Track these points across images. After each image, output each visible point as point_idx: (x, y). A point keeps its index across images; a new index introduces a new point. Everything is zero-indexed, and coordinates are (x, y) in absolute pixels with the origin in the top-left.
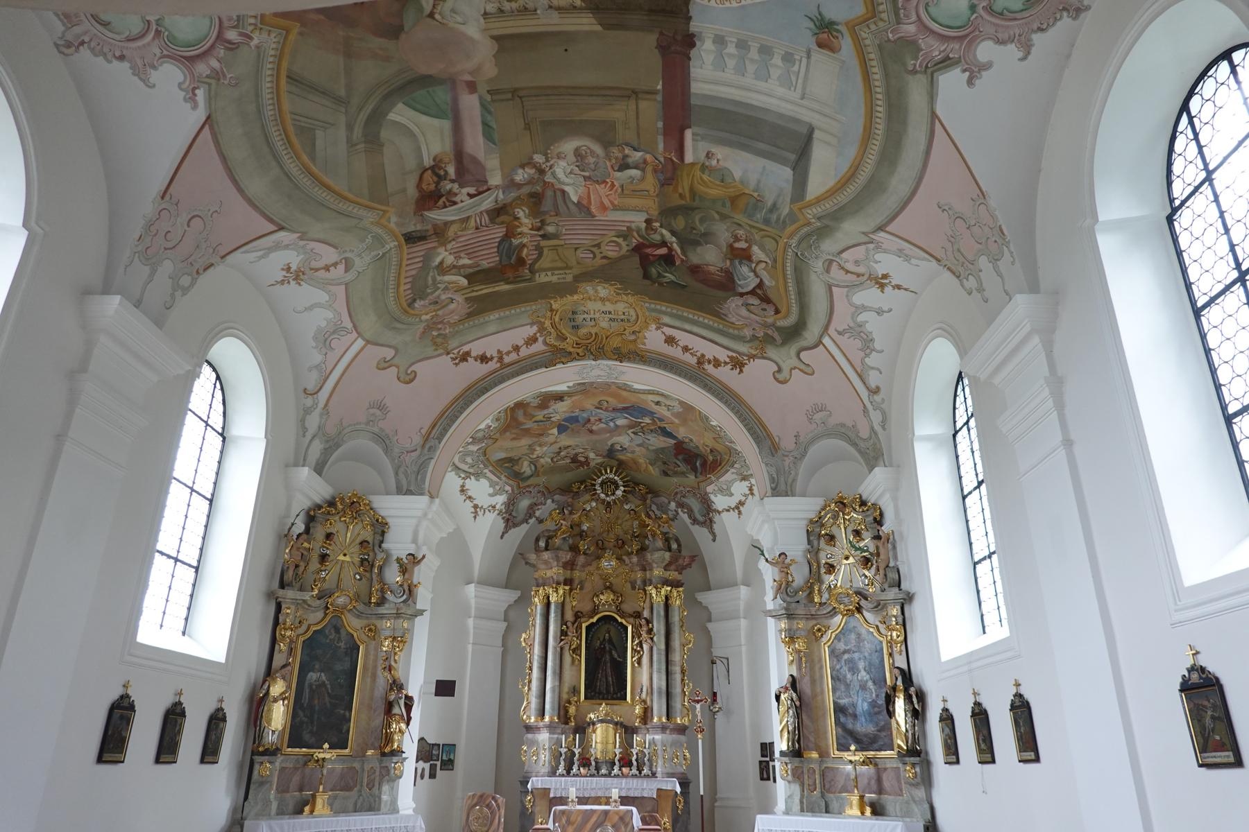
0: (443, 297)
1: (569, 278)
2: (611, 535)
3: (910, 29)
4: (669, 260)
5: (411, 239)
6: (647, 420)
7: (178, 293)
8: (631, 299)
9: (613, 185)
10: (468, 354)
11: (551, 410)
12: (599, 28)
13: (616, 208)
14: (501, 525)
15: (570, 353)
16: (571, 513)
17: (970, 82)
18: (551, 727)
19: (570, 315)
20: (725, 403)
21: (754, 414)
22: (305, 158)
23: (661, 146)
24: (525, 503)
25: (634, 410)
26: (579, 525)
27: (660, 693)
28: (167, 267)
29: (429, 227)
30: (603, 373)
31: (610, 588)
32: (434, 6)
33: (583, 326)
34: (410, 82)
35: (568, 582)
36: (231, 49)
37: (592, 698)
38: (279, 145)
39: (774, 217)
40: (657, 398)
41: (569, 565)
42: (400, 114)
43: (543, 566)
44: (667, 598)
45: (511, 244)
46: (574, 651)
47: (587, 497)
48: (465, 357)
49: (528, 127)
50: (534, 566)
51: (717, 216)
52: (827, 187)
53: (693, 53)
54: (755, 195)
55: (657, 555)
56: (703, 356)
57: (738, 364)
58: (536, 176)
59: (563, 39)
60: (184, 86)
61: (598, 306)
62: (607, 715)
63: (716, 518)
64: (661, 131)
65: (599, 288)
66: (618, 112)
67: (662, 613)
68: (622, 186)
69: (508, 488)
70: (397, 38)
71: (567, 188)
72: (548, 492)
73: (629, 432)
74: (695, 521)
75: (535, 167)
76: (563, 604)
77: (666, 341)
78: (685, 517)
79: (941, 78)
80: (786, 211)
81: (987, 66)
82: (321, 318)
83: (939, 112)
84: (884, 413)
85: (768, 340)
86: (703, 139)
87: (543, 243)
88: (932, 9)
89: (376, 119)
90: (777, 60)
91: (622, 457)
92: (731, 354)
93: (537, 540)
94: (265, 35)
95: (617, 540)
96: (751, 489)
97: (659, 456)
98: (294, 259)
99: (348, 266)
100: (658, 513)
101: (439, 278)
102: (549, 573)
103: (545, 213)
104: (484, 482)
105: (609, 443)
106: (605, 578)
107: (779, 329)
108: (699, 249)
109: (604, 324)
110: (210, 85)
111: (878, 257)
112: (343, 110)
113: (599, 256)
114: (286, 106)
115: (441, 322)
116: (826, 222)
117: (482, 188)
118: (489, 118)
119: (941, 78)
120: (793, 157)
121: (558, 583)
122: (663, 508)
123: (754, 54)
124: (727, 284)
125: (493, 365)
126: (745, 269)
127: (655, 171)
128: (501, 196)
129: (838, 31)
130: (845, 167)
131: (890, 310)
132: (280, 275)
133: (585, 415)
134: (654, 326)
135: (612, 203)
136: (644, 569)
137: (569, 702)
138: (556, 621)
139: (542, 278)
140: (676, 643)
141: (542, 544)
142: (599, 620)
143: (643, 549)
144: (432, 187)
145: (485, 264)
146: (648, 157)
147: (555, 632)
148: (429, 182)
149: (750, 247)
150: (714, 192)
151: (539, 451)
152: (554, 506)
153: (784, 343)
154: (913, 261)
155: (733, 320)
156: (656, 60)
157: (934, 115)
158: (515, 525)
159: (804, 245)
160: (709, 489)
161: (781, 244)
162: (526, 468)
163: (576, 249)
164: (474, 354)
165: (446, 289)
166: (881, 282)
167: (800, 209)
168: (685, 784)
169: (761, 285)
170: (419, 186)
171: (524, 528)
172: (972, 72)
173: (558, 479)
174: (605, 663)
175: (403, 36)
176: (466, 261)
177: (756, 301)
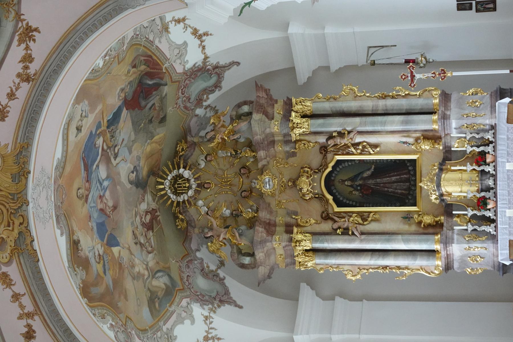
2: (236, 181)
6: (100, 142)
11: (90, 255)
14: (227, 308)
15: (20, 233)
16: (211, 229)
18: (447, 242)
20: (75, 48)
21: (88, 14)
24: (202, 283)
25: (88, 158)
26: (225, 219)
27: (406, 123)
30: (44, 194)
31: (294, 182)
35: (289, 229)
37: (415, 198)
40: (73, 131)
41: (270, 228)
43: (272, 258)
44: (304, 116)
46: (364, 220)
47: (192, 210)
50: (272, 269)
55: (256, 128)
56: (19, 75)
57: (28, 34)
62: (431, 181)
63: (213, 61)
67: (320, 121)
69: (184, 302)
72: (188, 257)
73: (114, 162)
74: (217, 86)
76: (313, 234)
78: (212, 97)
91: (144, 172)
93: (243, 266)
95: (241, 175)
96: (178, 21)
97: (143, 128)
100: (209, 128)
102: (280, 251)
104: (178, 331)
105: (129, 186)
106: (283, 187)
121: (291, 240)
122: (203, 122)
125: (37, 324)
133: (95, 215)
136: (273, 143)
137: (420, 223)
138: (332, 241)
140: (353, 105)
141: (247, 260)
142: (330, 193)
143: (250, 145)
147: (345, 241)
151: (139, 268)
152: (204, 249)
158: (227, 292)
160: (179, 69)
162: (160, 282)
168: (502, 94)
171: (230, 282)
173: (173, 245)
174: (377, 184)
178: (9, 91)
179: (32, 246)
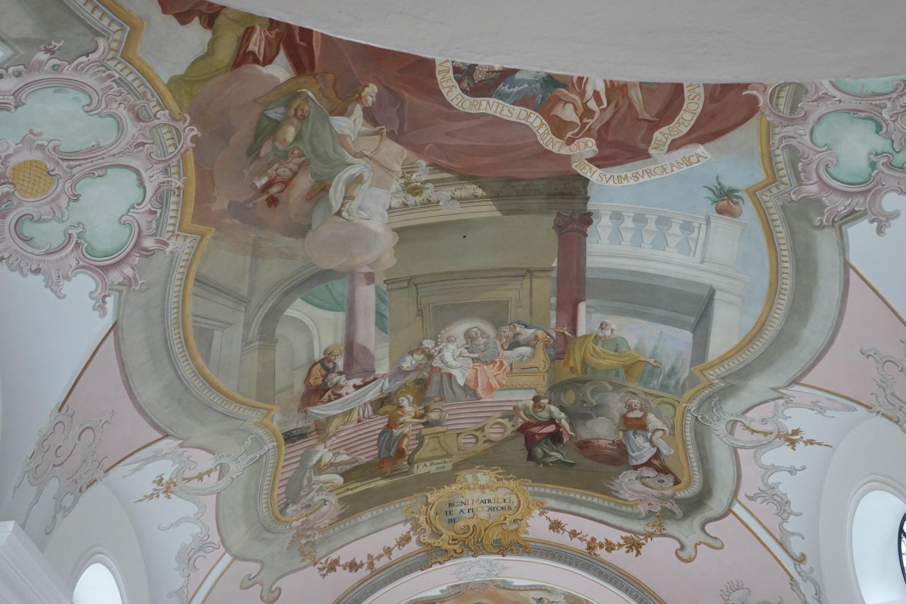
0: (316, 499)
1: (449, 467)
3: (812, 189)
4: (556, 438)
5: (291, 437)
7: (59, 516)
8: (513, 484)
9: (502, 364)
10: (336, 562)
12: (498, 214)
13: (503, 388)
15: (446, 551)
17: (880, 231)
19: (446, 508)
20: (626, 591)
22: (200, 360)
23: (553, 322)
28: (53, 486)
29: (311, 423)
32: (342, 205)
33: (460, 519)
34: (312, 277)
36: (147, 256)
38: (176, 347)
39: (673, 382)
42: (298, 309)
45: (392, 434)
48: (332, 567)
49: (420, 313)
51: (610, 387)
52: (730, 347)
53: (590, 230)
54: (652, 361)
56: (593, 539)
57: (634, 545)
58: (424, 362)
59: (463, 226)
60: (95, 295)
61: (477, 495)
65: (479, 475)
66: (512, 292)
70: (304, 237)
71: (453, 372)
75: (423, 352)
77: (551, 527)
79: (849, 230)
80: (686, 374)
81: (895, 215)
82: (186, 534)
83: (852, 261)
84: (815, 583)
85: (667, 514)
86: (597, 311)
87: (426, 431)
88: (831, 170)
89: (274, 315)
90: (675, 229)
92: (624, 534)
94: (181, 239)
98: (166, 468)
99: (223, 470)
101: (314, 478)
103: (430, 399)
107: (679, 501)
108: (589, 423)
109: (483, 514)
110: (121, 292)
111: (787, 412)
112: (243, 309)
113: (482, 440)
114: (190, 308)
115: (312, 528)
116: (731, 381)
117: (369, 377)
118: (383, 307)
119: (849, 230)
120: (692, 320)
123: (651, 225)
124: (619, 458)
125: (363, 572)
126: (639, 440)
127: (546, 346)
128: (387, 385)
130: (750, 324)
132: (150, 488)
134: (537, 512)
135: (500, 383)
139: (421, 469)
144: (320, 381)
145: (363, 459)
146: (540, 333)
148: (317, 378)
149: (645, 416)
150: (607, 363)
153: (686, 516)
154: (828, 413)
155: (626, 496)
156: (552, 240)
157: (847, 266)
159: (705, 407)
161: (680, 410)
163: (458, 435)
164: (342, 562)
165: (321, 489)
166: (791, 439)
167: (701, 371)
169: (657, 455)
170: (306, 381)
172: (880, 222)
175: (310, 235)
176: (345, 457)
177: (651, 473)
179: (435, 563)
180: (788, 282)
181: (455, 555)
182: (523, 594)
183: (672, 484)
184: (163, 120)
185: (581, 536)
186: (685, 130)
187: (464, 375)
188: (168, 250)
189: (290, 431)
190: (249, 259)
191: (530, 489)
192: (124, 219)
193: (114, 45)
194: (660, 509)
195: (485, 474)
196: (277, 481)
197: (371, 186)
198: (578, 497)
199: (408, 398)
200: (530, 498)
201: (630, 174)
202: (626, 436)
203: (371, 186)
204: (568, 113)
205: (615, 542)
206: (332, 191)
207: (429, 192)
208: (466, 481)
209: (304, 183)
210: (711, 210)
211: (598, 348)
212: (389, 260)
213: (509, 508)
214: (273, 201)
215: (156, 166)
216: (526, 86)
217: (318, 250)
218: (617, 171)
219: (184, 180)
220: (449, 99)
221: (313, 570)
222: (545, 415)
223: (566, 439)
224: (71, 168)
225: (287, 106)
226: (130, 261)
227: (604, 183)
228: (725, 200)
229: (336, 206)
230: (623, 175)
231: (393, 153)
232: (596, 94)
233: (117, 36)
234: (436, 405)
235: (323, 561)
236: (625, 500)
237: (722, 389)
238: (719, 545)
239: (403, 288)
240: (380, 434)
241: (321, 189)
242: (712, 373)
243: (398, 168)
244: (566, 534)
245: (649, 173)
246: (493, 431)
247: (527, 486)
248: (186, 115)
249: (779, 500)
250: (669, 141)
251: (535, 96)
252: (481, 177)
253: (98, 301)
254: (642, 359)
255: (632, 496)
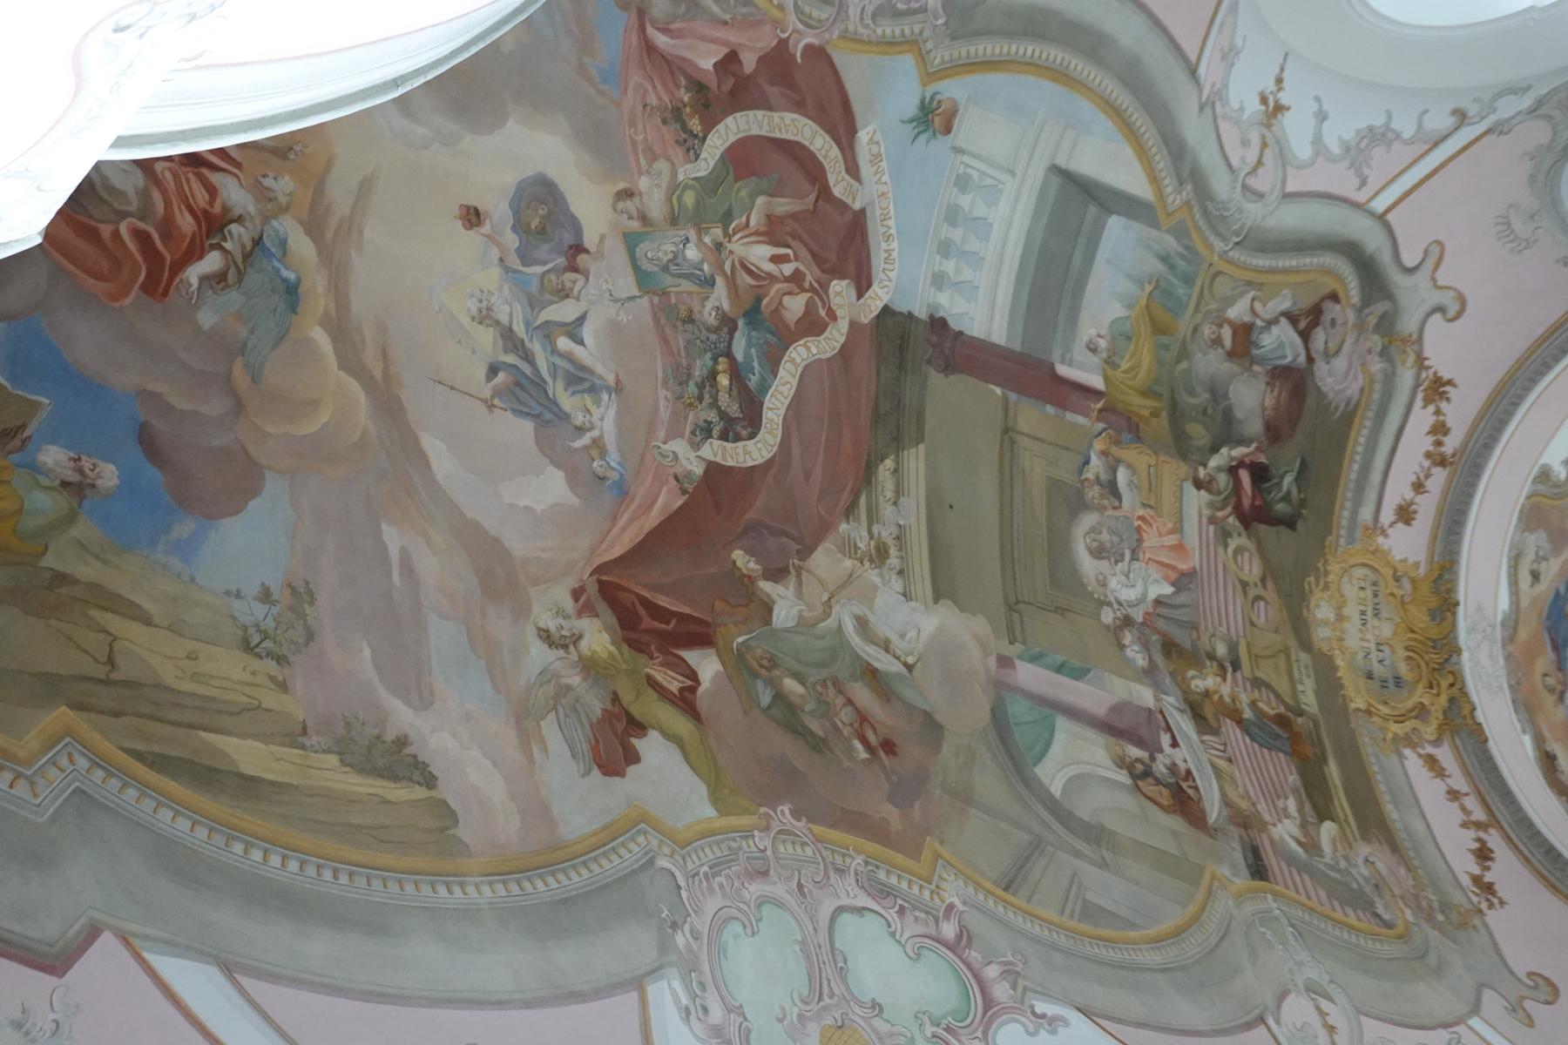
1: (1304, 657)
5: (1259, 870)
8: (1334, 568)
9: (1141, 518)
10: (1477, 880)
12: (922, 447)
13: (1178, 529)
15: (1452, 700)
19: (1375, 685)
20: (1516, 405)
22: (1133, 934)
23: (1081, 420)
32: (898, 658)
36: (970, 939)
39: (1181, 264)
49: (1061, 611)
51: (1184, 365)
52: (1136, 162)
53: (954, 324)
54: (1148, 288)
56: (1428, 455)
57: (1437, 389)
61: (1353, 626)
64: (1060, 411)
65: (1319, 616)
66: (1036, 467)
68: (1145, 505)
84: (1501, 94)
85: (1386, 325)
90: (965, 201)
92: (1419, 403)
107: (1366, 302)
108: (1239, 414)
109: (1386, 630)
110: (1026, 989)
113: (1260, 591)
114: (1052, 914)
116: (1185, 174)
120: (1093, 210)
123: (956, 234)
124: (1294, 382)
125: (1494, 840)
127: (1118, 443)
128: (1171, 699)
129: (932, 99)
130: (1104, 124)
131: (1317, 99)
134: (1381, 540)
135: (1170, 532)
145: (1293, 779)
146: (1098, 445)
149: (1230, 323)
150: (1147, 360)
161: (1223, 266)
163: (1252, 624)
164: (1476, 870)
165: (1346, 858)
176: (1291, 804)
178: (1413, 478)
179: (1473, 718)
180: (1053, 54)
181: (1458, 686)
182: (1525, 602)
183: (1338, 307)
184: (767, 843)
185: (1422, 476)
186: (835, 151)
187: (1155, 581)
188: (960, 907)
189: (1249, 867)
190: (973, 811)
191: (1342, 541)
192: (910, 952)
193: (666, 850)
194: (1376, 338)
195: (1318, 606)
196: (1334, 915)
197: (871, 608)
198: (1356, 467)
199: (1194, 677)
200: (1357, 546)
201: (884, 245)
202: (1259, 361)
203: (871, 608)
204: (795, 305)
205: (1431, 420)
206: (876, 665)
207: (886, 533)
208: (1329, 639)
209: (863, 695)
210: (944, 142)
211: (1125, 365)
212: (980, 625)
213: (1375, 584)
214: (889, 746)
215: (832, 881)
216: (753, 350)
217: (966, 718)
218: (878, 261)
219: (857, 853)
220: (760, 461)
221: (1492, 917)
222: (1223, 480)
223: (1262, 459)
224: (832, 995)
225: (755, 675)
226: (977, 966)
227: (892, 285)
228: (934, 119)
229: (896, 667)
230: (884, 255)
231: (825, 561)
232: (776, 259)
233: (655, 843)
234: (1205, 640)
235: (1475, 899)
236: (1362, 390)
237: (1196, 190)
238: (1436, 250)
239: (1022, 621)
240: (1253, 739)
241: (871, 675)
242: (1171, 199)
243: (848, 563)
244: (1419, 499)
245: (885, 217)
246: (1247, 567)
247: (1338, 546)
248: (763, 810)
249: (1365, 142)
250: (847, 177)
251: (767, 343)
252: (869, 455)
253: (1041, 1026)
254: (1144, 302)
255: (1355, 378)
